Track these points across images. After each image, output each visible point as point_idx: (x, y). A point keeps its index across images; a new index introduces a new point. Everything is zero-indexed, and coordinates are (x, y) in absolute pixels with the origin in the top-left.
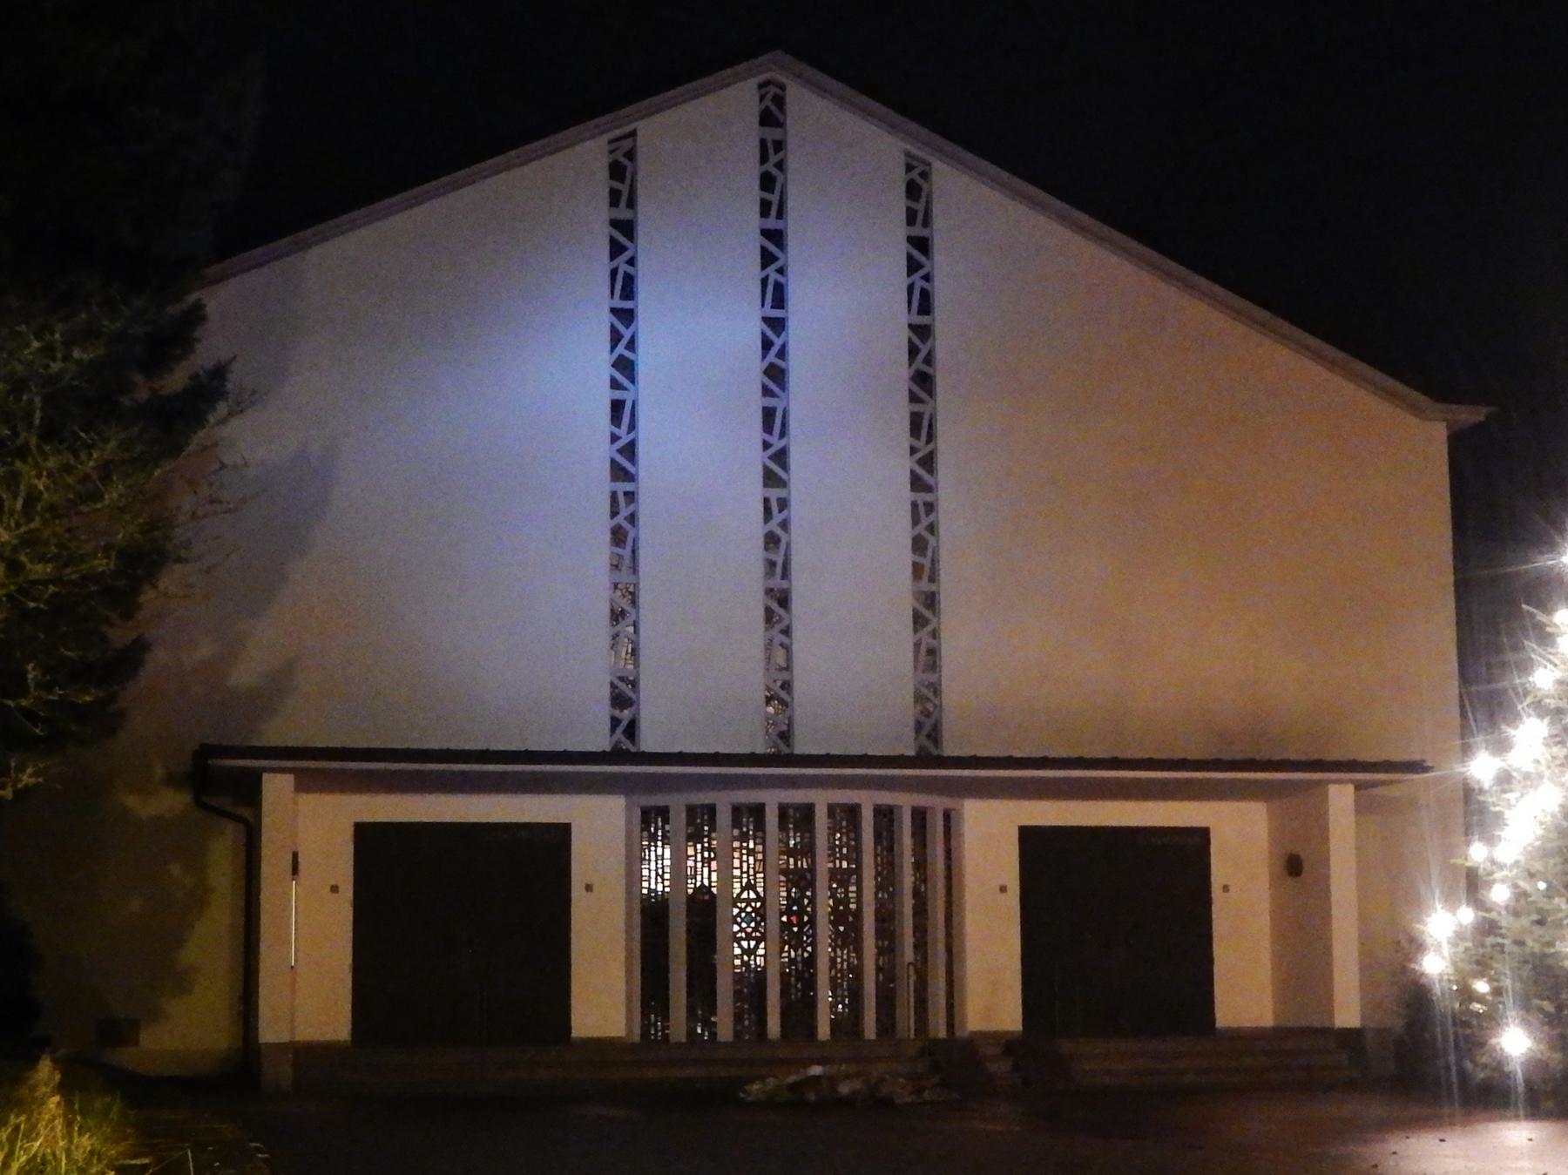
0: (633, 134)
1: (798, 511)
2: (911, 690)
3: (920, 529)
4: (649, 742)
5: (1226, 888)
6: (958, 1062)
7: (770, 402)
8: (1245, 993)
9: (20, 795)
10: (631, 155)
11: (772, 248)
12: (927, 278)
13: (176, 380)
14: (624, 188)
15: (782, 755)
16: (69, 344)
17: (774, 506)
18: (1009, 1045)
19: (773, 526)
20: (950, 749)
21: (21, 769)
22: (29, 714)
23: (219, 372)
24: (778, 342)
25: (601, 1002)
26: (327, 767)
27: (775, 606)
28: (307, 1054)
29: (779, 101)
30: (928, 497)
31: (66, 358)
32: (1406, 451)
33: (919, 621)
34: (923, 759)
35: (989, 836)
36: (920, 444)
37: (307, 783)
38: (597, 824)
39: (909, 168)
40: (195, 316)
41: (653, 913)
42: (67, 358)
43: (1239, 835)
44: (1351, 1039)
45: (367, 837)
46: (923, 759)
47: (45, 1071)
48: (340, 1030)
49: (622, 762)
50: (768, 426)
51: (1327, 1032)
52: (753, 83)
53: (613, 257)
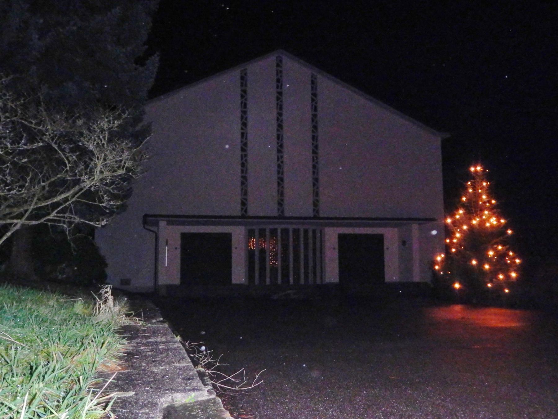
0: (246, 69)
1: (249, 158)
2: (240, 201)
3: (279, 162)
4: (250, 213)
5: (388, 249)
6: (326, 288)
7: (279, 133)
8: (392, 273)
9: (103, 226)
10: (246, 74)
11: (244, 94)
12: (246, 100)
13: (138, 128)
14: (280, 85)
15: (281, 217)
16: (114, 120)
17: (244, 156)
18: (335, 285)
19: (244, 161)
20: (321, 215)
21: (103, 220)
22: (105, 207)
23: (149, 125)
24: (245, 116)
25: (239, 275)
26: (174, 219)
27: (280, 181)
28: (169, 287)
29: (281, 61)
30: (245, 153)
31: (113, 123)
32: (425, 145)
33: (314, 185)
34: (315, 217)
35: (331, 235)
36: (279, 141)
37: (169, 223)
38: (238, 233)
39: (312, 77)
40: (143, 113)
41: (251, 254)
42: (113, 123)
43: (391, 236)
44: (418, 284)
45: (184, 236)
46: (315, 217)
47: (107, 290)
48: (176, 280)
49: (243, 218)
50: (278, 139)
51: (413, 283)
52: (274, 58)
53: (277, 100)
